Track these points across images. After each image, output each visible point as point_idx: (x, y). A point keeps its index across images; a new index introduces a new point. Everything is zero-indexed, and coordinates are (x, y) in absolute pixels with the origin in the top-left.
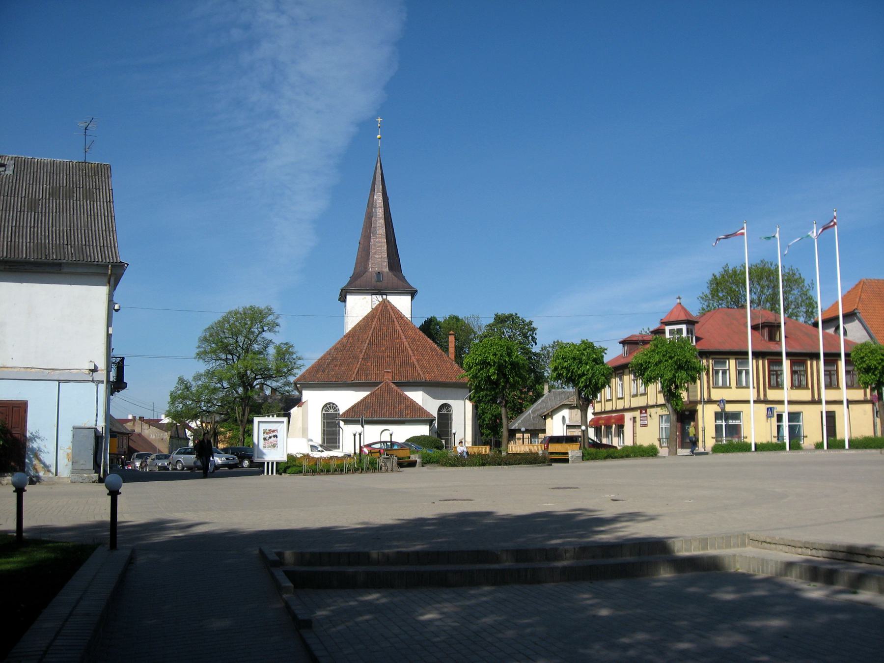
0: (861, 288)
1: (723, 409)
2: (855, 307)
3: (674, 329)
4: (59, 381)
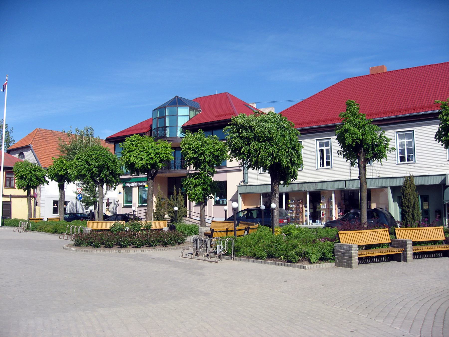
0: (35, 133)
1: (392, 233)
2: (30, 143)
3: (407, 156)
4: (345, 181)
